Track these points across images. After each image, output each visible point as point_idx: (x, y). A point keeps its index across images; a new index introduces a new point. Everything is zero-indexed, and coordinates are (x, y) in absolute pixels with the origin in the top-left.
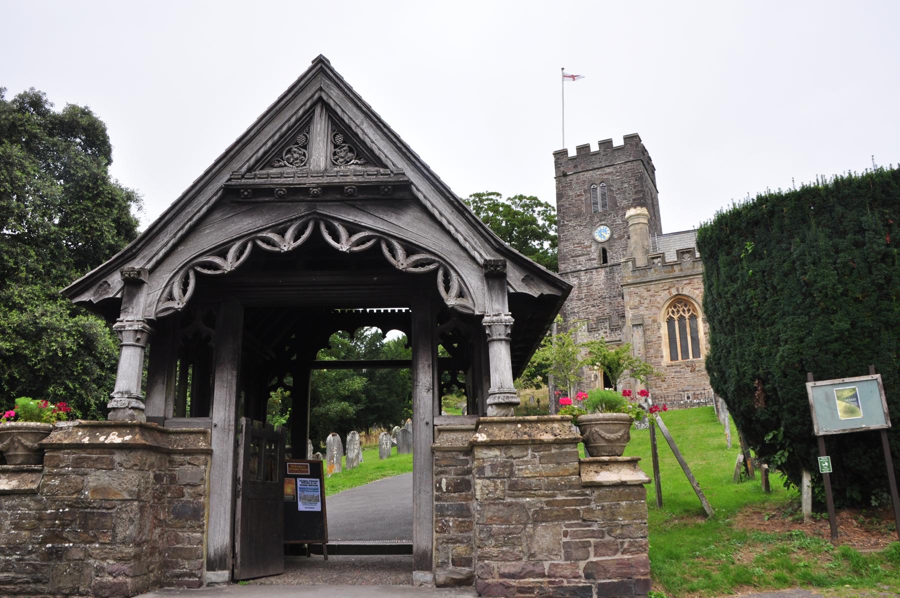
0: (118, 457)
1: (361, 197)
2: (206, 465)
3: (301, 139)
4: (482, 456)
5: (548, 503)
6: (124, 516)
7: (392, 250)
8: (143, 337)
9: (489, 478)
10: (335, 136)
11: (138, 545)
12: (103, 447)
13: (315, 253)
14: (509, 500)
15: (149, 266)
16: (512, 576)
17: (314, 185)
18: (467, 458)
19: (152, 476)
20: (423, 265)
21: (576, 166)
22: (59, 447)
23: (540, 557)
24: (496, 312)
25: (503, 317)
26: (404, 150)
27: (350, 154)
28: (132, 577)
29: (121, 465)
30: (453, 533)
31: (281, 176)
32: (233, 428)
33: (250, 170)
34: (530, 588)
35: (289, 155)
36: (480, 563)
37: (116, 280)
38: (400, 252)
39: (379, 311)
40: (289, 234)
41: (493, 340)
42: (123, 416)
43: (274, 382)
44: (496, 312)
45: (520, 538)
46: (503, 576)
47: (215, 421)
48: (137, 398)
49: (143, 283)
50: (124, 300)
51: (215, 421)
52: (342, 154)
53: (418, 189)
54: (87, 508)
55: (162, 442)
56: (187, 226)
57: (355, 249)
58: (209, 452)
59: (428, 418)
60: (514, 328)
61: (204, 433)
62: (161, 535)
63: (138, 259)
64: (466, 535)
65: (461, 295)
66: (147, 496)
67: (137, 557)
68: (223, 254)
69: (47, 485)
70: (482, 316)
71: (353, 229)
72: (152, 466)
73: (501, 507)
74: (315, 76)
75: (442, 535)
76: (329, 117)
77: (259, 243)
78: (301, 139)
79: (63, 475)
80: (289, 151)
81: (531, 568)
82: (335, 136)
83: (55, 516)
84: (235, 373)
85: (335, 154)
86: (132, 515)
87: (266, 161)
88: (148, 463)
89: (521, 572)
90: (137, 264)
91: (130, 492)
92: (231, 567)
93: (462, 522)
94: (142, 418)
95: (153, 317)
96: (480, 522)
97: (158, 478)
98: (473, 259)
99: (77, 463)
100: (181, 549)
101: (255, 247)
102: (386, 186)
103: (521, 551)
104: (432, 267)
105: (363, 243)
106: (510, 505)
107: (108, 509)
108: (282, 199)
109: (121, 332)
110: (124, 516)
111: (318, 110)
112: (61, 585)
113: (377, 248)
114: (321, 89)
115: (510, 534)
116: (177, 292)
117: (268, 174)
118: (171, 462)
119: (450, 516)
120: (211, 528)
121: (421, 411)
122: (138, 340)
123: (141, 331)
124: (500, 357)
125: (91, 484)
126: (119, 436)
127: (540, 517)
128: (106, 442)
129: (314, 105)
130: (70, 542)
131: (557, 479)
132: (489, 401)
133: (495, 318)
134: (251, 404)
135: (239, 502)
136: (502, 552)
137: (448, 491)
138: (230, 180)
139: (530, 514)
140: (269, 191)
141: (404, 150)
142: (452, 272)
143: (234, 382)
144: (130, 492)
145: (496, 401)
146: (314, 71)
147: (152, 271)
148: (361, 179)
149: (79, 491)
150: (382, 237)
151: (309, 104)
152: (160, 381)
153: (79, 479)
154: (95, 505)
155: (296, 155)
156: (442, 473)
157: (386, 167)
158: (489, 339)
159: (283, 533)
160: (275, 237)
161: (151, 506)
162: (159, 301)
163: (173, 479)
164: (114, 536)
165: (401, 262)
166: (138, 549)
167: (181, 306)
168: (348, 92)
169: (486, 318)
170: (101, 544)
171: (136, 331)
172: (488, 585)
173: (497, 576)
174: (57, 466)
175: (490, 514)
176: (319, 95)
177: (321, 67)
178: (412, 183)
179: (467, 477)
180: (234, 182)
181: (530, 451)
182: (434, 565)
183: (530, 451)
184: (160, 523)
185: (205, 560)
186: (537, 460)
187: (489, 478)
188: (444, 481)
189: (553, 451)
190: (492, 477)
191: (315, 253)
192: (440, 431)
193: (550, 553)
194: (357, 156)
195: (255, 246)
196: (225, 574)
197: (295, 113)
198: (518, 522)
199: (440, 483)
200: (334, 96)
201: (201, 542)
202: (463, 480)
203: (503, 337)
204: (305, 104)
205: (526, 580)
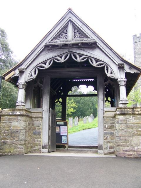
0: (19, 118)
1: (82, 46)
2: (41, 121)
3: (65, 31)
4: (118, 118)
5: (136, 131)
6: (21, 133)
7: (92, 61)
8: (25, 86)
9: (120, 124)
10: (74, 30)
11: (25, 141)
12: (15, 115)
13: (71, 63)
14: (126, 130)
15: (26, 67)
16: (126, 151)
17: (70, 44)
18: (114, 119)
19: (28, 123)
20: (100, 65)
21: (139, 40)
22: (4, 115)
23: (134, 146)
24: (121, 77)
25: (123, 79)
26: (94, 33)
27: (79, 35)
28: (24, 149)
29: (20, 120)
30: (109, 140)
31: (60, 41)
32: (48, 111)
33: (52, 40)
34: (131, 154)
35: (62, 36)
36: (117, 147)
37: (17, 71)
38: (94, 62)
39: (83, 81)
40: (63, 57)
41: (121, 86)
42: (21, 107)
43: (57, 100)
44: (121, 77)
45: (129, 140)
46: (124, 151)
47: (43, 109)
48: (24, 103)
49: (24, 72)
50: (19, 77)
51: (43, 109)
52: (77, 35)
53: (98, 44)
54: (12, 131)
55: (30, 115)
56: (42, 49)
57: (81, 61)
58: (42, 118)
59: (102, 108)
60: (127, 82)
61: (41, 112)
62: (30, 139)
63: (22, 66)
64: (113, 140)
65: (111, 73)
66: (27, 128)
67: (25, 144)
68: (45, 64)
69: (2, 125)
70: (117, 79)
71: (80, 55)
72: (28, 121)
73: (123, 132)
74: (68, 14)
75: (106, 140)
76: (73, 25)
77: (55, 60)
78: (65, 31)
79: (6, 123)
80: (62, 35)
81: (131, 149)
82: (74, 30)
83: (4, 133)
84: (49, 96)
85: (75, 35)
86: (23, 133)
87: (55, 38)
88: (27, 120)
89: (129, 150)
90: (22, 67)
91: (23, 127)
92: (48, 148)
93: (112, 137)
94: (24, 108)
95: (27, 81)
96: (118, 136)
97: (29, 124)
98: (115, 63)
99: (9, 120)
100: (36, 143)
101: (54, 61)
102: (90, 43)
103: (129, 144)
104: (103, 65)
105: (84, 59)
106: (126, 131)
107: (17, 131)
108: (61, 48)
109: (19, 85)
110: (21, 133)
111: (70, 23)
112: (6, 150)
113: (87, 61)
114: (70, 17)
115: (126, 139)
116: (33, 74)
117: (57, 41)
118: (32, 120)
119: (109, 135)
120: (43, 138)
121: (100, 106)
122: (23, 87)
123: (24, 85)
124: (123, 90)
125: (13, 125)
126: (19, 113)
127: (134, 135)
128: (16, 114)
129: (68, 22)
130: (8, 140)
131: (139, 124)
132: (120, 102)
133: (121, 79)
134: (52, 105)
135: (50, 131)
136: (124, 144)
137: (108, 128)
138: (46, 43)
139: (132, 134)
140: (57, 46)
141: (94, 33)
142: (109, 66)
143: (48, 99)
144: (23, 127)
145: (122, 102)
146: (68, 12)
147: (26, 69)
148: (82, 42)
149: (10, 127)
150: (89, 57)
151: (67, 22)
152: (29, 98)
153: (10, 123)
154: (14, 130)
155: (64, 36)
156: (106, 123)
157: (89, 38)
158: (120, 85)
159: (57, 143)
160: (59, 58)
161: (28, 131)
162: (28, 77)
163: (33, 125)
164: (19, 139)
165: (94, 64)
166: (25, 142)
167: (34, 78)
168: (78, 18)
169: (118, 80)
170: (16, 140)
171: (23, 85)
172: (120, 153)
173: (122, 151)
174: (4, 120)
175: (120, 134)
176: (70, 21)
177: (70, 11)
178: (97, 42)
179: (113, 124)
180: (47, 44)
181: (131, 116)
182: (104, 149)
183: (131, 116)
184: (30, 136)
185: (41, 146)
186: (133, 119)
187: (120, 124)
188: (107, 126)
189: (138, 116)
190: (121, 124)
191: (71, 63)
192: (105, 112)
193: (137, 145)
194: (81, 35)
195: (54, 61)
196: (47, 150)
197: (63, 24)
198: (128, 136)
199: (106, 126)
200: (74, 19)
201: (41, 141)
202: (112, 125)
203: (124, 85)
204: (66, 21)
205: (130, 152)
